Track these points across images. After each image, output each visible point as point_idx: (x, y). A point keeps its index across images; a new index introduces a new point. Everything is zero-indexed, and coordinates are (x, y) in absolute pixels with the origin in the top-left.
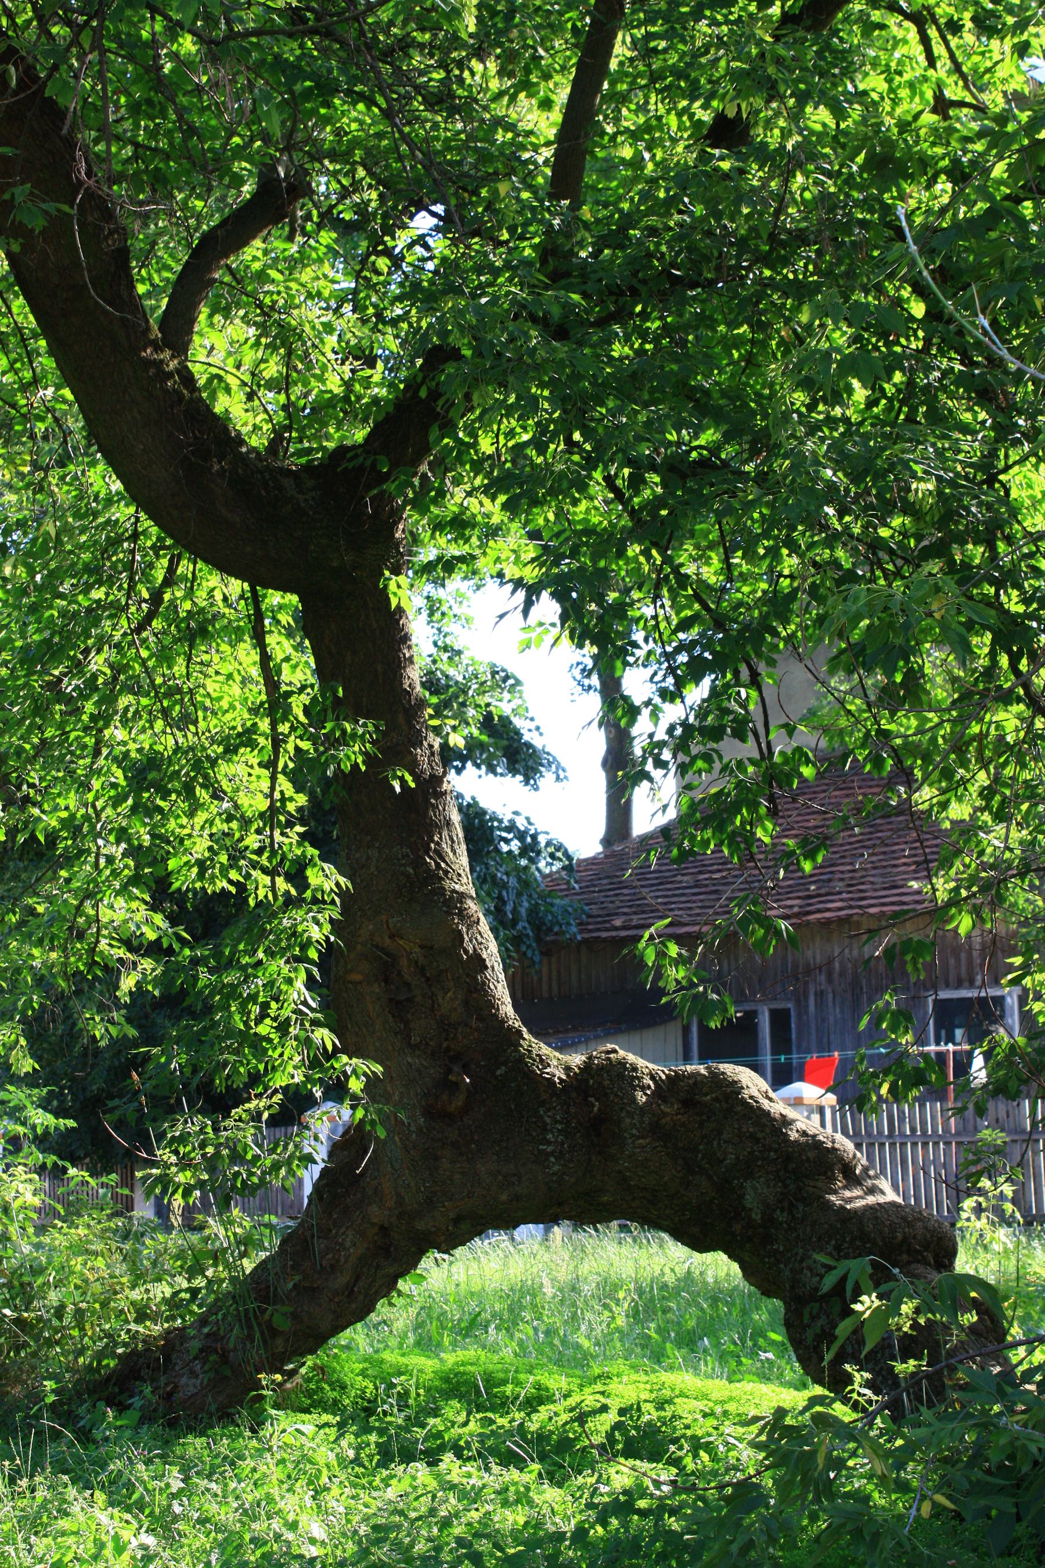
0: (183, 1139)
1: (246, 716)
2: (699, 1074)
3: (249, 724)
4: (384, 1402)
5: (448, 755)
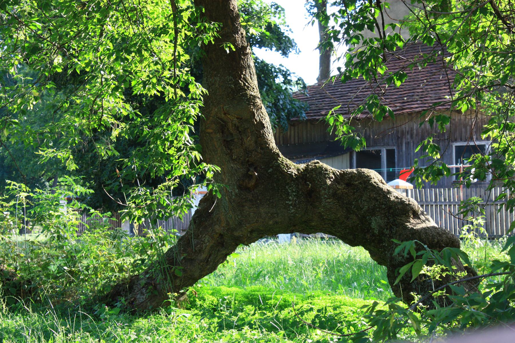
0: (138, 197)
1: (164, 20)
2: (353, 172)
3: (164, 24)
4: (221, 306)
5: (252, 41)
